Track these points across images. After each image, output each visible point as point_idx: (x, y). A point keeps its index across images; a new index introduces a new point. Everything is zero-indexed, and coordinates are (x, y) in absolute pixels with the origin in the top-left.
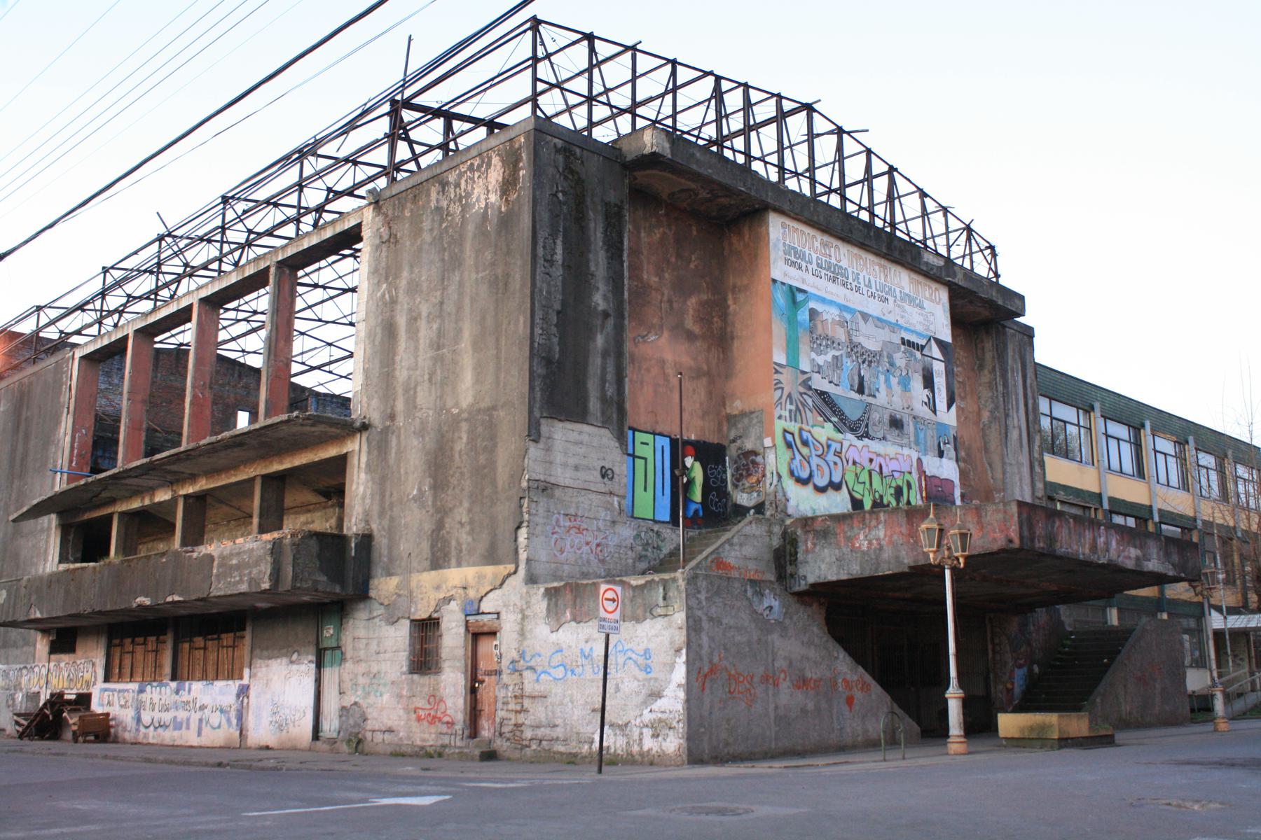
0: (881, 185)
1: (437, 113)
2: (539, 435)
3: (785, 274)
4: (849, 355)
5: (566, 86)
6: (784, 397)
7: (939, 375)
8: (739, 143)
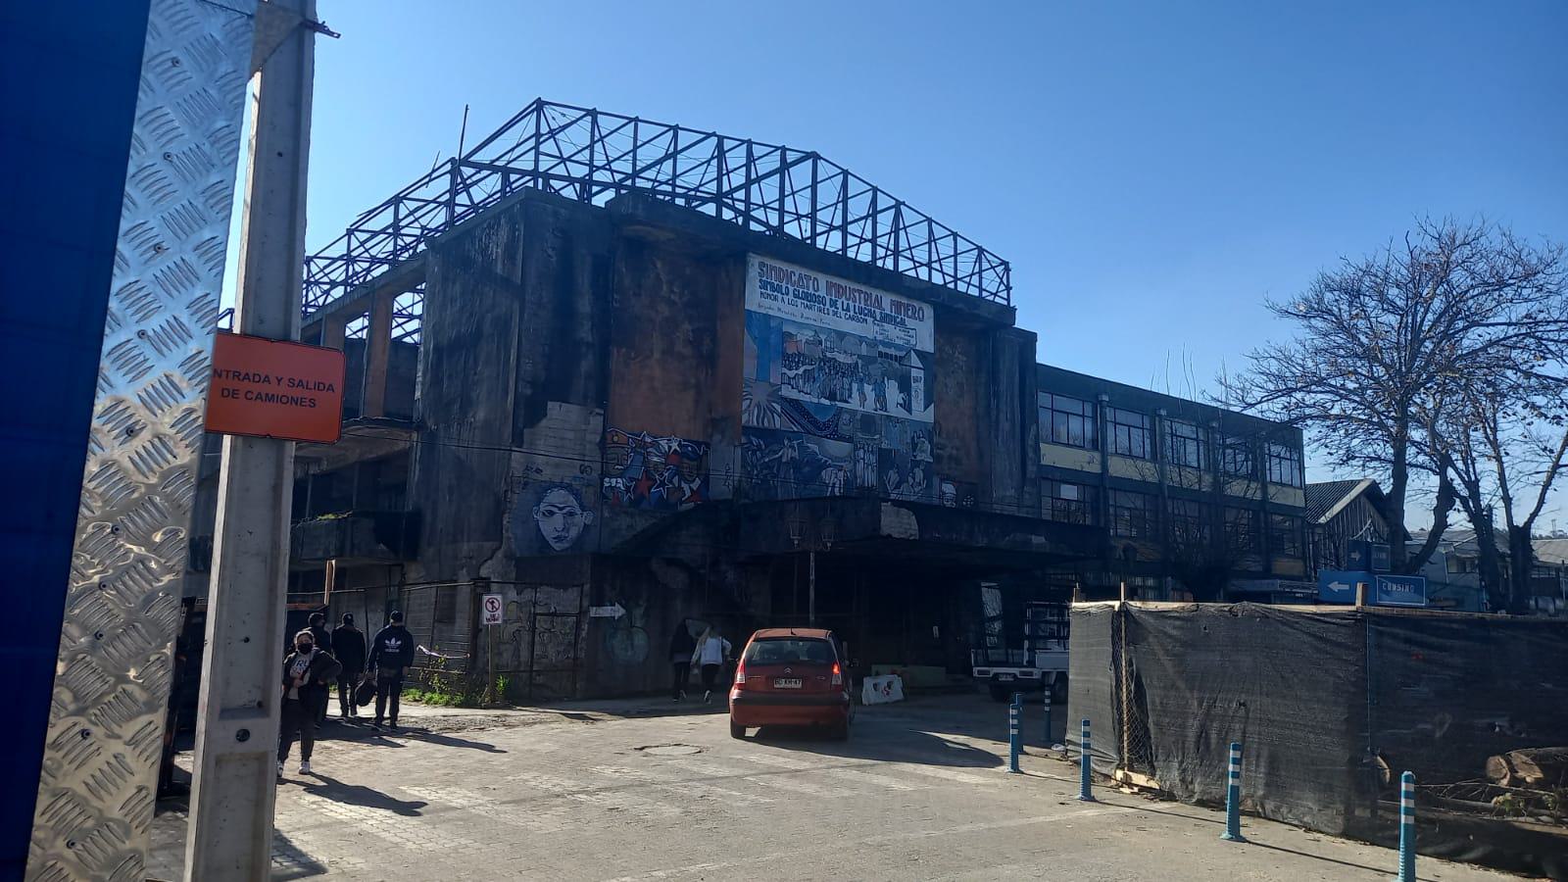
1: (492, 167)
2: (522, 442)
3: (760, 306)
5: (557, 161)
8: (740, 195)
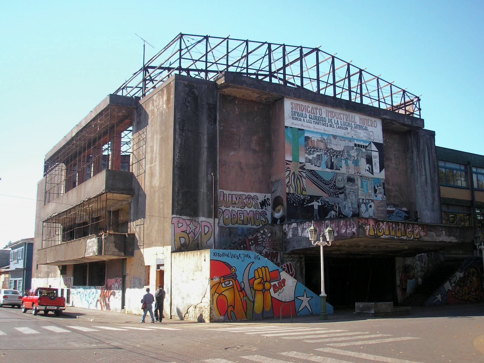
0: (355, 80)
4: (326, 154)
6: (291, 174)
7: (375, 158)
